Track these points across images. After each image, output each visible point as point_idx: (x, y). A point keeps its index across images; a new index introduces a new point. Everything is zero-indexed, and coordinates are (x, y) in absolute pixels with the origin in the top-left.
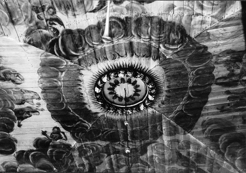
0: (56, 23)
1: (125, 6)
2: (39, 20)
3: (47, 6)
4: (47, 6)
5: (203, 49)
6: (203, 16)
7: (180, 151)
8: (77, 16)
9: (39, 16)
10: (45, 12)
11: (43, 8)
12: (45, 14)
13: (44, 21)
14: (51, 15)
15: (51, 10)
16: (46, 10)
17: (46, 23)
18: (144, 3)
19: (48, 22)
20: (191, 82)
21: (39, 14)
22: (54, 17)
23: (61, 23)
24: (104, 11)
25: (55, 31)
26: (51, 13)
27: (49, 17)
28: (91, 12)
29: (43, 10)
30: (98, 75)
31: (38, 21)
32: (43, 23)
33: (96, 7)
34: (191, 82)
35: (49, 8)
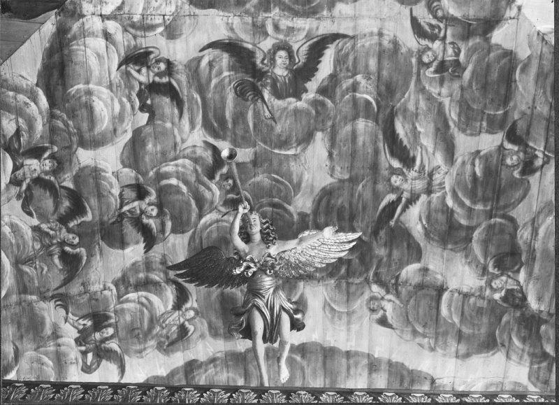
0: (427, 28)
1: (269, 38)
2: (459, 45)
3: (432, 69)
4: (432, 69)
5: (482, 261)
6: (101, 15)
7: (235, 74)
8: (376, 30)
9: (455, 52)
10: (440, 58)
11: (442, 67)
12: (441, 54)
13: (449, 39)
14: (429, 49)
15: (425, 59)
16: (435, 64)
17: (449, 32)
18: (228, 41)
19: (442, 34)
20: (250, 95)
21: (455, 58)
22: (425, 42)
23: (414, 22)
24: (315, 33)
25: (435, 7)
26: (430, 53)
27: (437, 45)
28: (344, 36)
29: (442, 63)
30: (298, 122)
31: (461, 43)
32: (453, 36)
33: (330, 46)
34: (250, 95)
35: (428, 65)
